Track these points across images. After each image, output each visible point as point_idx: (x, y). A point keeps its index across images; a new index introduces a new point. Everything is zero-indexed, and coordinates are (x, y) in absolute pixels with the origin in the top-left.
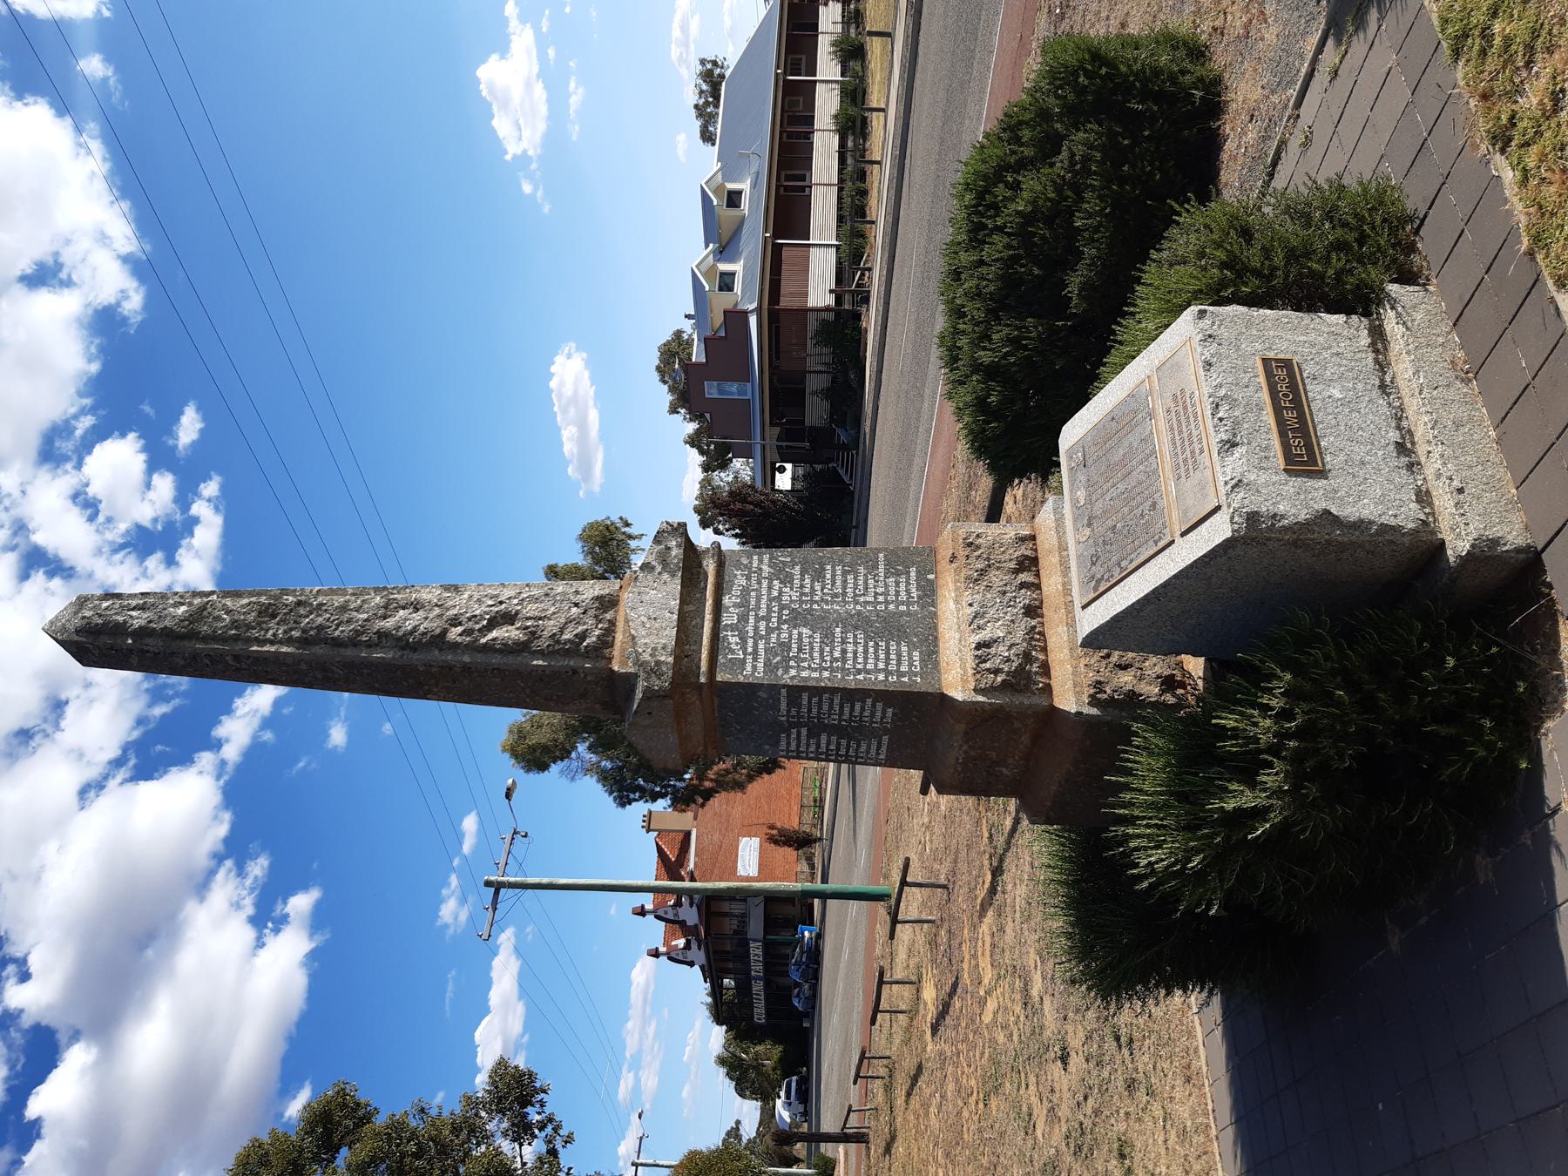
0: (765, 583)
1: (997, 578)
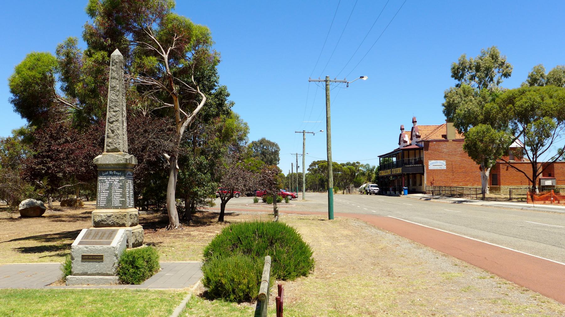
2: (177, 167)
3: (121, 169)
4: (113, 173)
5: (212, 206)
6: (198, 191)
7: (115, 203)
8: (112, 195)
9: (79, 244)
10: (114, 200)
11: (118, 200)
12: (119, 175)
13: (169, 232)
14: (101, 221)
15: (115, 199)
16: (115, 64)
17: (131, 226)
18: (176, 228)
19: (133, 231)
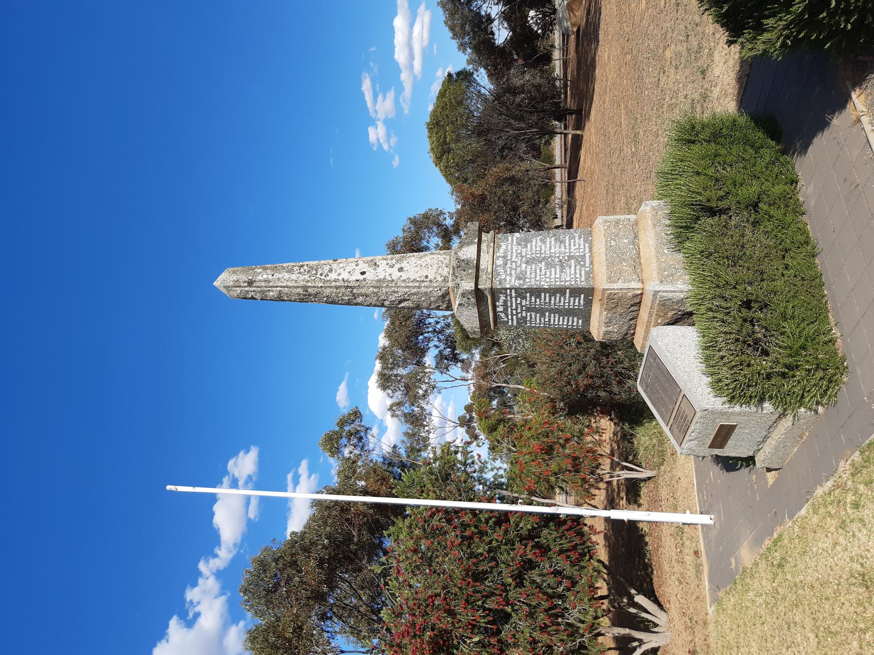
0: (514, 299)
1: (620, 310)
4: (501, 305)
11: (569, 300)
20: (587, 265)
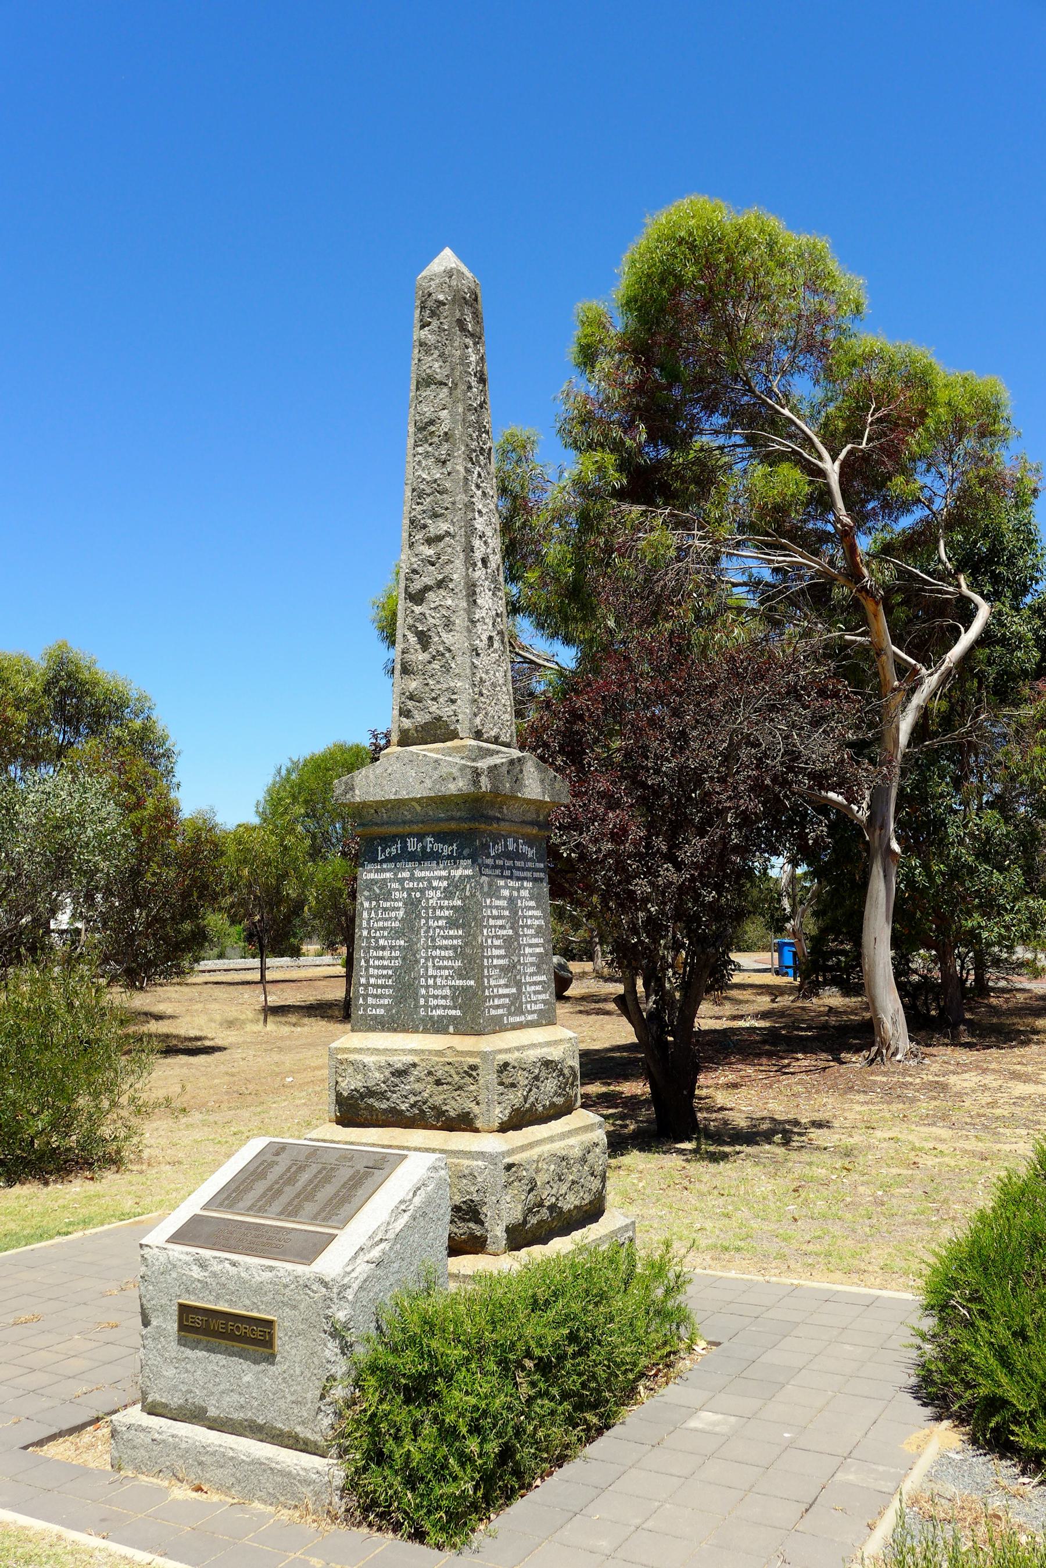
2: (895, 846)
3: (453, 825)
4: (424, 848)
5: (1036, 978)
6: (980, 927)
7: (433, 1002)
8: (417, 961)
9: (178, 1238)
10: (427, 987)
11: (443, 987)
12: (449, 857)
13: (872, 1074)
14: (362, 1096)
15: (431, 982)
16: (433, 314)
17: (503, 1128)
18: (899, 1057)
19: (509, 1160)
20: (512, 1019)
